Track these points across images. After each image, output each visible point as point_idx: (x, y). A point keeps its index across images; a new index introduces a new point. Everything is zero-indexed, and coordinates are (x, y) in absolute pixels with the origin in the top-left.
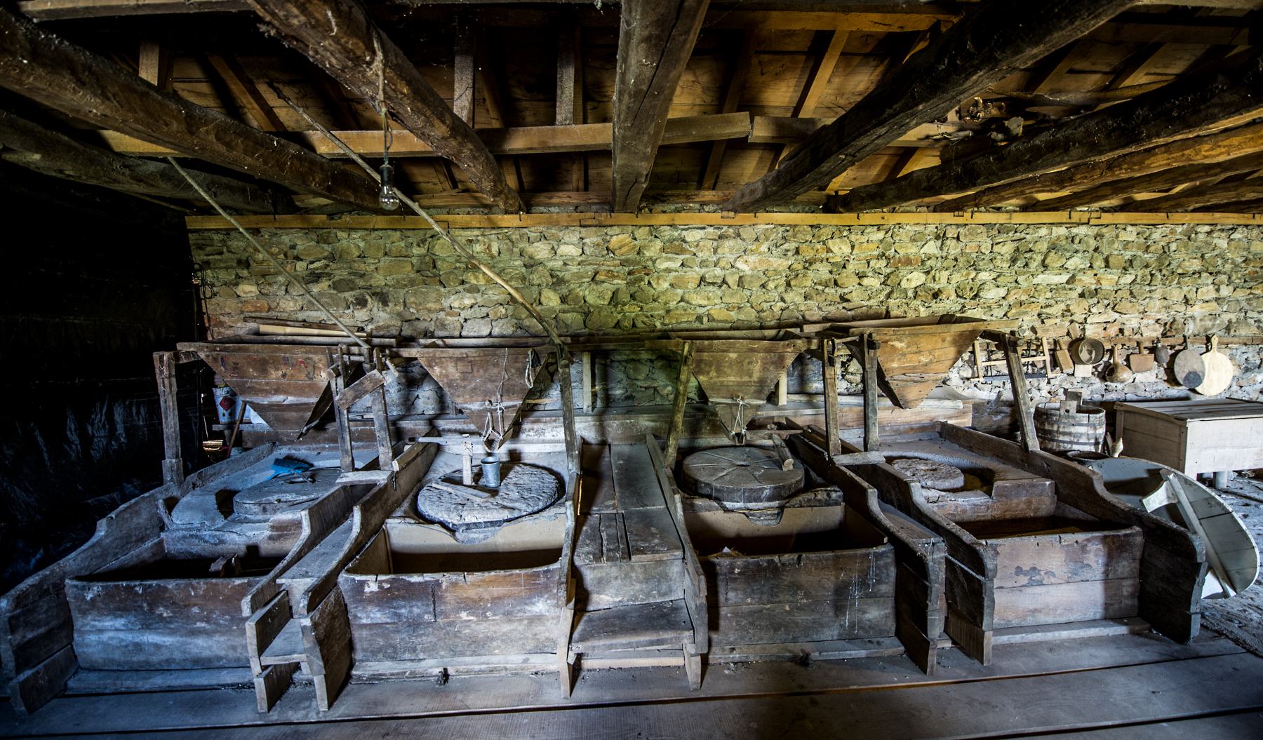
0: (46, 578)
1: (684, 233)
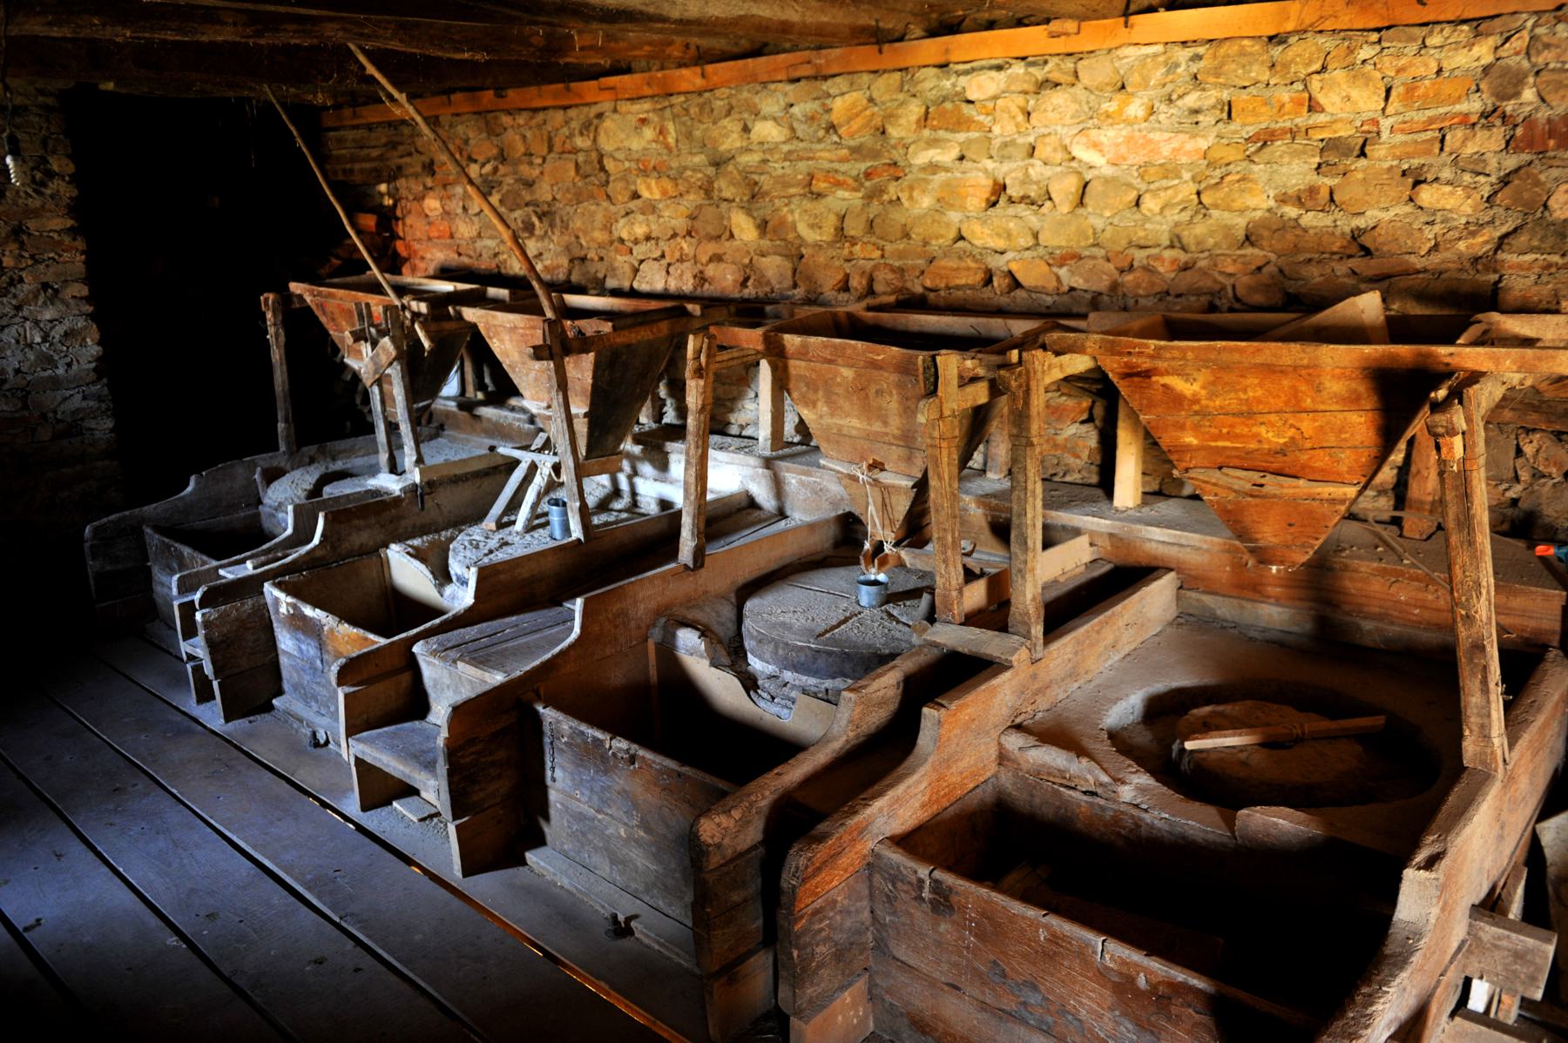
0: (125, 518)
1: (963, 80)
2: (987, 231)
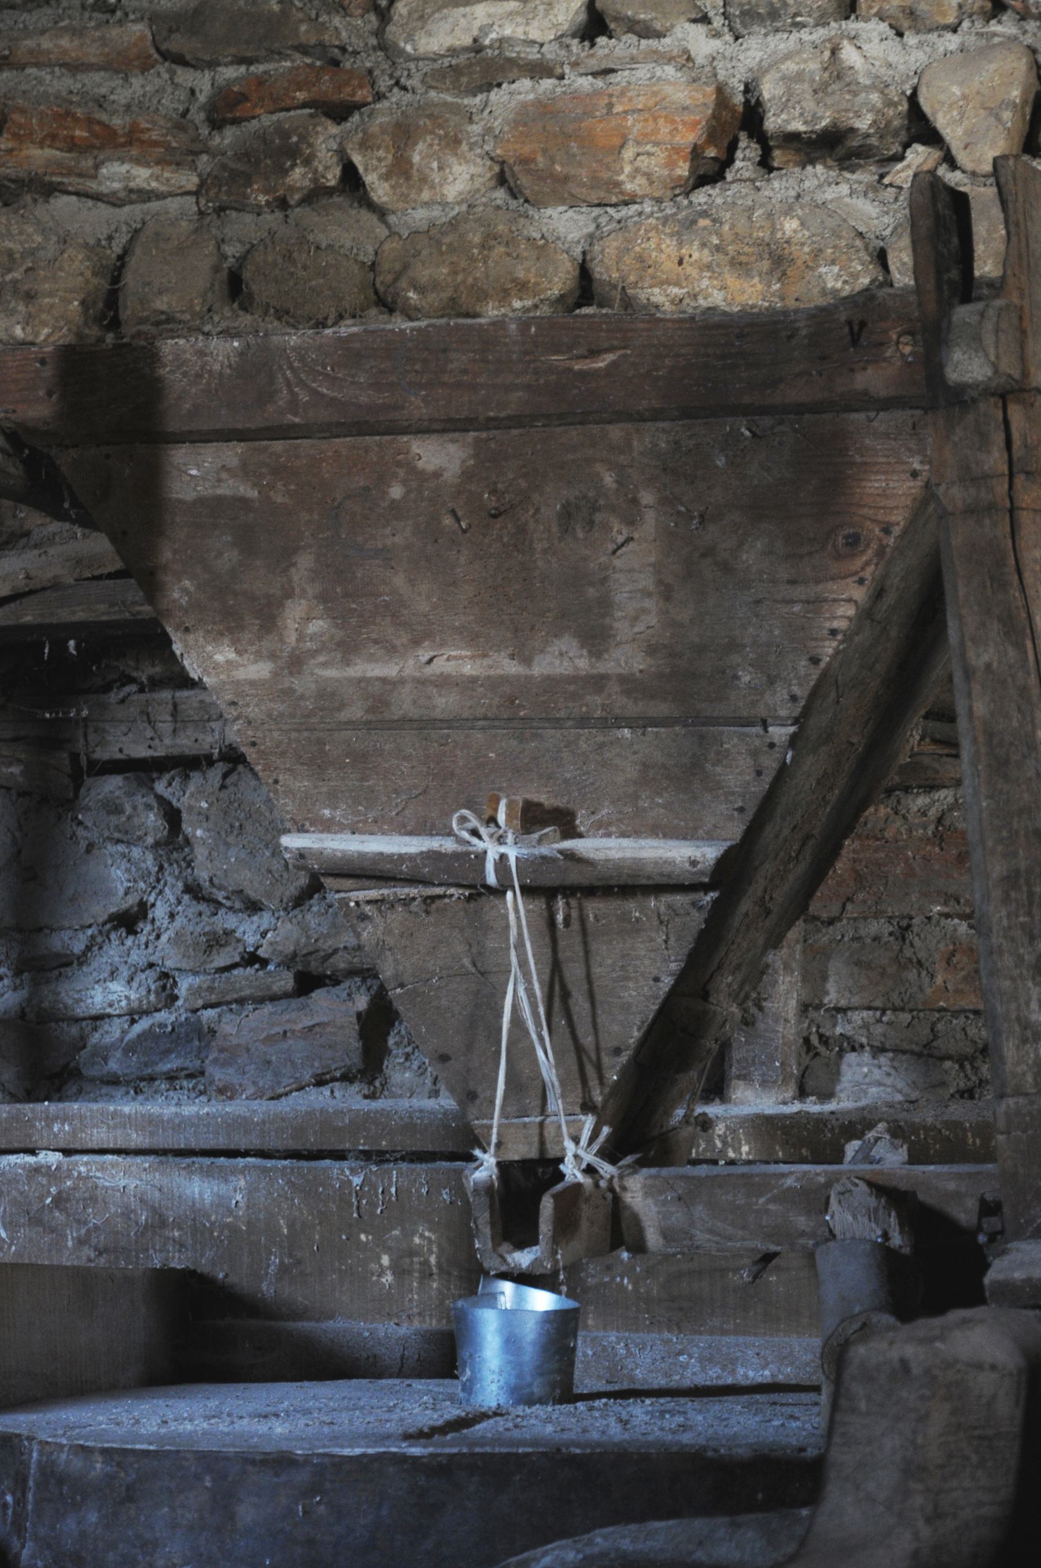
2: (697, 254)
